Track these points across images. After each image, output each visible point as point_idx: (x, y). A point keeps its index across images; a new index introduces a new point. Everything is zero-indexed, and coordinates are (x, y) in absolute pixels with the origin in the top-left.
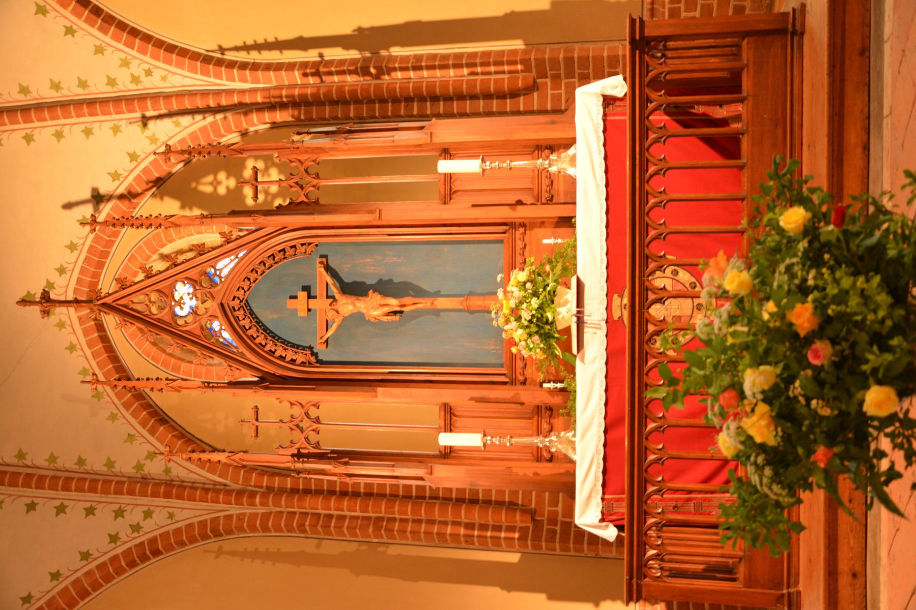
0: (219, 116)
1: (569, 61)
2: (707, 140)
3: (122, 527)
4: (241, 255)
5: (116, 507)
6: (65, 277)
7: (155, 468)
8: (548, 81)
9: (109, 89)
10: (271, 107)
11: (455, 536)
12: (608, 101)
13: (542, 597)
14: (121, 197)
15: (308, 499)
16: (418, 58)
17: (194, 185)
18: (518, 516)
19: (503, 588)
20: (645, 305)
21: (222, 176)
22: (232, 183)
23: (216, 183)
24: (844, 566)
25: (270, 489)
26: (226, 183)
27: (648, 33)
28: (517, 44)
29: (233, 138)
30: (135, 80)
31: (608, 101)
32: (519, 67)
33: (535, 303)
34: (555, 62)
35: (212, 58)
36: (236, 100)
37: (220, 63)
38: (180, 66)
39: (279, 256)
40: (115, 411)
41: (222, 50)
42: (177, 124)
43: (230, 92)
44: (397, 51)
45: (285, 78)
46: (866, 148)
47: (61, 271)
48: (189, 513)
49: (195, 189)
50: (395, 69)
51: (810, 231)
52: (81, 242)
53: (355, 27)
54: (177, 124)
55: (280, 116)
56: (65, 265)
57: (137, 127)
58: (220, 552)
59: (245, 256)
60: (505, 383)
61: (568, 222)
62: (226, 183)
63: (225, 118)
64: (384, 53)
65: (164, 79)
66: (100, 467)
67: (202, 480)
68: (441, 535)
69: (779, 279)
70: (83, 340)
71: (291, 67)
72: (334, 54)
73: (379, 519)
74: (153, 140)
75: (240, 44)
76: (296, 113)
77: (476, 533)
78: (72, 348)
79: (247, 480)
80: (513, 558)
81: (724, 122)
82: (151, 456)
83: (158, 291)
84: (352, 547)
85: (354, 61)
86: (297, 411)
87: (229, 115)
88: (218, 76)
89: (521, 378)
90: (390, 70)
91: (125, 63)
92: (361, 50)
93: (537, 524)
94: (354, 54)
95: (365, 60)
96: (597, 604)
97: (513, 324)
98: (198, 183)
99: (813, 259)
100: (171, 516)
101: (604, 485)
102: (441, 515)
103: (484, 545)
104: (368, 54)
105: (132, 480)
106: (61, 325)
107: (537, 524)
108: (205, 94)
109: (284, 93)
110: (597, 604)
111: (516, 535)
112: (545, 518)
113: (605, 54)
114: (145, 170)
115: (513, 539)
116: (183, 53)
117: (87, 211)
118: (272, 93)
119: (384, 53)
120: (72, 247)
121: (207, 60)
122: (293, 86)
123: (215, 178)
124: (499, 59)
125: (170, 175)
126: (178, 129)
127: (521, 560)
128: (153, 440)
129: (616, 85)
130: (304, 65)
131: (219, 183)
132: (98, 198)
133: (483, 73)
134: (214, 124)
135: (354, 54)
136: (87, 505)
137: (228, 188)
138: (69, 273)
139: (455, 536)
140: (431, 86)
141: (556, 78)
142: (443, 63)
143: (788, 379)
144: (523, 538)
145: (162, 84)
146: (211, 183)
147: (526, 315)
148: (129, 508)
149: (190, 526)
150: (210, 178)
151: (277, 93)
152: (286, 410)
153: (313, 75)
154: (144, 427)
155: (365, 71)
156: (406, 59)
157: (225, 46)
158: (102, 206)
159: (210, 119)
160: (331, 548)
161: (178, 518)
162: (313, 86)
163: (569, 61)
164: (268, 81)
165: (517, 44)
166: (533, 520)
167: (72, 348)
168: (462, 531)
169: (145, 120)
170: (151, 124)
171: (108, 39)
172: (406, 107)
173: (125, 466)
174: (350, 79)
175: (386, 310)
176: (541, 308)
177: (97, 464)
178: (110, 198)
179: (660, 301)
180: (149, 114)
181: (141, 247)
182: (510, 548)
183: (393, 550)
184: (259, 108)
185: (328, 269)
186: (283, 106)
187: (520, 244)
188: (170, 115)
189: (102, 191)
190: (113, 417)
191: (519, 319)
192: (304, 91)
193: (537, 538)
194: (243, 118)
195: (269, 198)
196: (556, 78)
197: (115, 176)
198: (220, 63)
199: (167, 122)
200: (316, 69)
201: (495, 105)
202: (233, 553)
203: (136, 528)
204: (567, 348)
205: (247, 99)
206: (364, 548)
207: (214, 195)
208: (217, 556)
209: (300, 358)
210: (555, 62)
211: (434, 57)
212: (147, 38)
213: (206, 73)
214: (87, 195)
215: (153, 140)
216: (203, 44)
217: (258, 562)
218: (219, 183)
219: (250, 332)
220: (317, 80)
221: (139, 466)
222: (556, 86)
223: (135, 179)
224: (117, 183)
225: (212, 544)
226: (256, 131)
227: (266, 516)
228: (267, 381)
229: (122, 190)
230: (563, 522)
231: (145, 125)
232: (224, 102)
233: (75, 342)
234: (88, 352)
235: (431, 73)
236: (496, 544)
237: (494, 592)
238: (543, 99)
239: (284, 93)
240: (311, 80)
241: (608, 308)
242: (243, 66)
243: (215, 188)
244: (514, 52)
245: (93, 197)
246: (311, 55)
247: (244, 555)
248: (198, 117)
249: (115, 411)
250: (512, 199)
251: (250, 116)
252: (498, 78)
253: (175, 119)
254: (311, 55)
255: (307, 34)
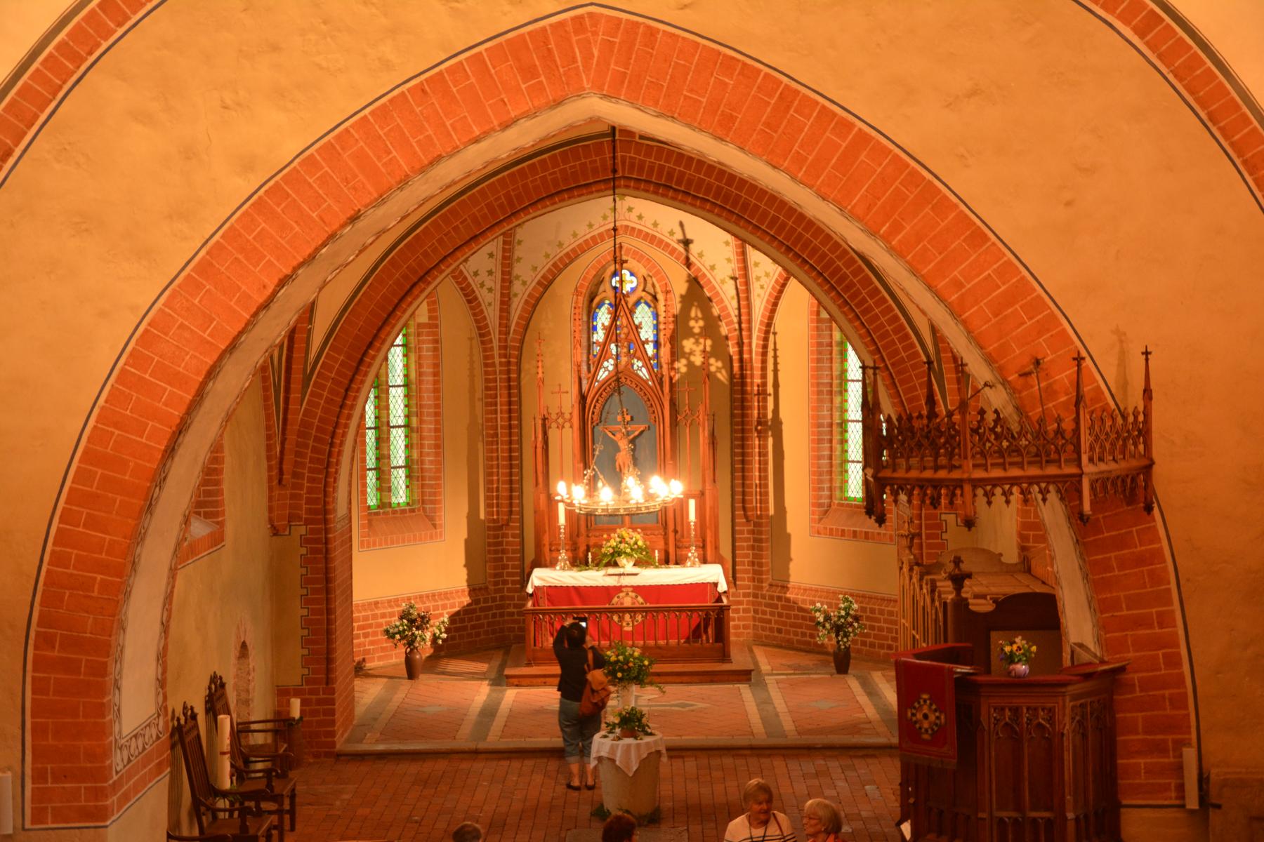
0: (737, 326)
1: (761, 541)
2: (699, 625)
3: (483, 276)
4: (650, 383)
5: (494, 270)
6: (636, 220)
7: (517, 287)
8: (752, 528)
9: (753, 263)
10: (741, 360)
11: (491, 482)
12: (716, 585)
13: (465, 536)
14: (687, 259)
15: (505, 392)
16: (766, 454)
17: (696, 304)
18: (506, 517)
19: (468, 514)
20: (629, 612)
21: (701, 323)
22: (697, 330)
23: (696, 319)
24: (547, 679)
25: (509, 363)
26: (696, 326)
27: (725, 612)
28: (772, 512)
29: (724, 330)
30: (758, 278)
31: (716, 585)
32: (759, 513)
33: (628, 550)
34: (760, 533)
35: (770, 327)
36: (746, 341)
37: (767, 332)
38: (765, 309)
39: (651, 410)
40: (551, 257)
41: (775, 334)
42: (733, 298)
43: (750, 337)
44: (770, 441)
45: (757, 373)
46: (682, 683)
47: (640, 217)
48: (492, 315)
49: (693, 305)
50: (759, 441)
51: (644, 665)
52: (659, 230)
53: (783, 421)
54: (733, 298)
55: (736, 365)
56: (644, 219)
57: (730, 273)
58: (471, 339)
59: (649, 385)
60: (587, 527)
61: (666, 561)
62: (696, 326)
63: (736, 330)
64: (770, 433)
65: (759, 296)
66: (517, 254)
67: (511, 318)
68: (491, 474)
69: (636, 661)
70: (595, 233)
71: (764, 376)
72: (770, 400)
73: (496, 435)
74: (723, 282)
75: (778, 347)
76: (738, 376)
77: (495, 494)
78: (590, 226)
79: (514, 348)
80: (482, 516)
81: (706, 632)
82: (524, 283)
83: (629, 333)
84: (480, 421)
85: (765, 415)
86: (567, 416)
87: (737, 333)
88: (760, 330)
89: (590, 535)
90: (759, 437)
91: (767, 275)
92: (772, 419)
93: (501, 528)
94: (770, 415)
95: (767, 422)
96: (465, 566)
97: (618, 540)
98: (697, 307)
99: (639, 666)
100: (490, 304)
101: (550, 586)
102: (503, 473)
103: (487, 498)
104: (770, 423)
105: (510, 273)
106: (605, 218)
107: (501, 528)
108: (749, 321)
109: (749, 372)
110: (465, 566)
111: (495, 517)
112: (504, 531)
113: (764, 561)
114: (704, 275)
115: (493, 515)
116: (773, 311)
117: (679, 236)
118: (749, 365)
119: (770, 433)
120: (655, 224)
121: (769, 325)
122: (752, 376)
123: (699, 319)
124: (764, 501)
125: (702, 287)
126: (729, 298)
127: (482, 520)
128: (534, 284)
129: (723, 587)
130: (764, 384)
131: (697, 321)
132: (686, 243)
133: (756, 491)
134: (732, 322)
135: (770, 415)
136: (495, 253)
137: (693, 327)
138: (638, 222)
139: (491, 482)
140: (750, 462)
141: (753, 532)
142: (763, 469)
143: (621, 663)
144: (494, 521)
145: (756, 294)
146: (696, 316)
147: (622, 546)
148: (493, 278)
149: (485, 318)
150: (700, 315)
151: (748, 368)
152: (567, 410)
153: (758, 390)
154: (542, 277)
155: (759, 423)
156: (766, 447)
157: (777, 336)
158: (682, 245)
159: (735, 320)
160: (479, 406)
161: (488, 307)
162: (752, 390)
163: (761, 541)
164: (757, 364)
165: (772, 512)
166: (503, 525)
167: (590, 226)
168: (495, 486)
169: (734, 279)
170: (732, 282)
171: (769, 290)
172: (738, 445)
173: (518, 269)
174: (756, 412)
175: (622, 464)
176: (625, 553)
177: (519, 252)
178: (687, 250)
179: (631, 617)
180: (738, 281)
181: (656, 267)
182: (487, 513)
183: (480, 446)
184: (741, 353)
185: (642, 433)
186: (742, 368)
187: (656, 532)
188: (738, 294)
189: (691, 246)
190: (547, 256)
191: (621, 542)
192: (749, 384)
193: (495, 529)
194: (736, 341)
195: (687, 356)
196: (753, 532)
197: (701, 255)
198: (767, 332)
199: (733, 292)
200: (762, 393)
201: (739, 497)
202: (471, 348)
203: (482, 285)
204: (608, 565)
205: (746, 348)
206: (480, 427)
207: (689, 318)
208: (469, 338)
209: (595, 417)
210: (760, 533)
211: (766, 463)
212: (781, 292)
213: (761, 323)
214: (689, 237)
215: (723, 282)
216: (777, 320)
217: (468, 359)
218: (697, 321)
219: (608, 389)
220: (756, 392)
221: (517, 277)
222: (749, 532)
223: (699, 267)
224: (696, 256)
225: (475, 333)
226: (728, 346)
227: (493, 365)
228: (583, 398)
229: (692, 259)
230: (502, 542)
231: (732, 278)
232: (744, 333)
233: (594, 227)
234: (588, 237)
235: (757, 462)
236: (488, 506)
237: (465, 509)
238: (742, 525)
239: (749, 372)
240: (756, 388)
241: (626, 586)
242: (765, 347)
243: (693, 319)
244: (767, 509)
245: (688, 240)
246: (770, 389)
247: (471, 355)
248: (736, 312)
249: (551, 257)
250: (679, 528)
251: (736, 346)
252: (754, 500)
253: (736, 297)
254: (770, 389)
255: (781, 390)
